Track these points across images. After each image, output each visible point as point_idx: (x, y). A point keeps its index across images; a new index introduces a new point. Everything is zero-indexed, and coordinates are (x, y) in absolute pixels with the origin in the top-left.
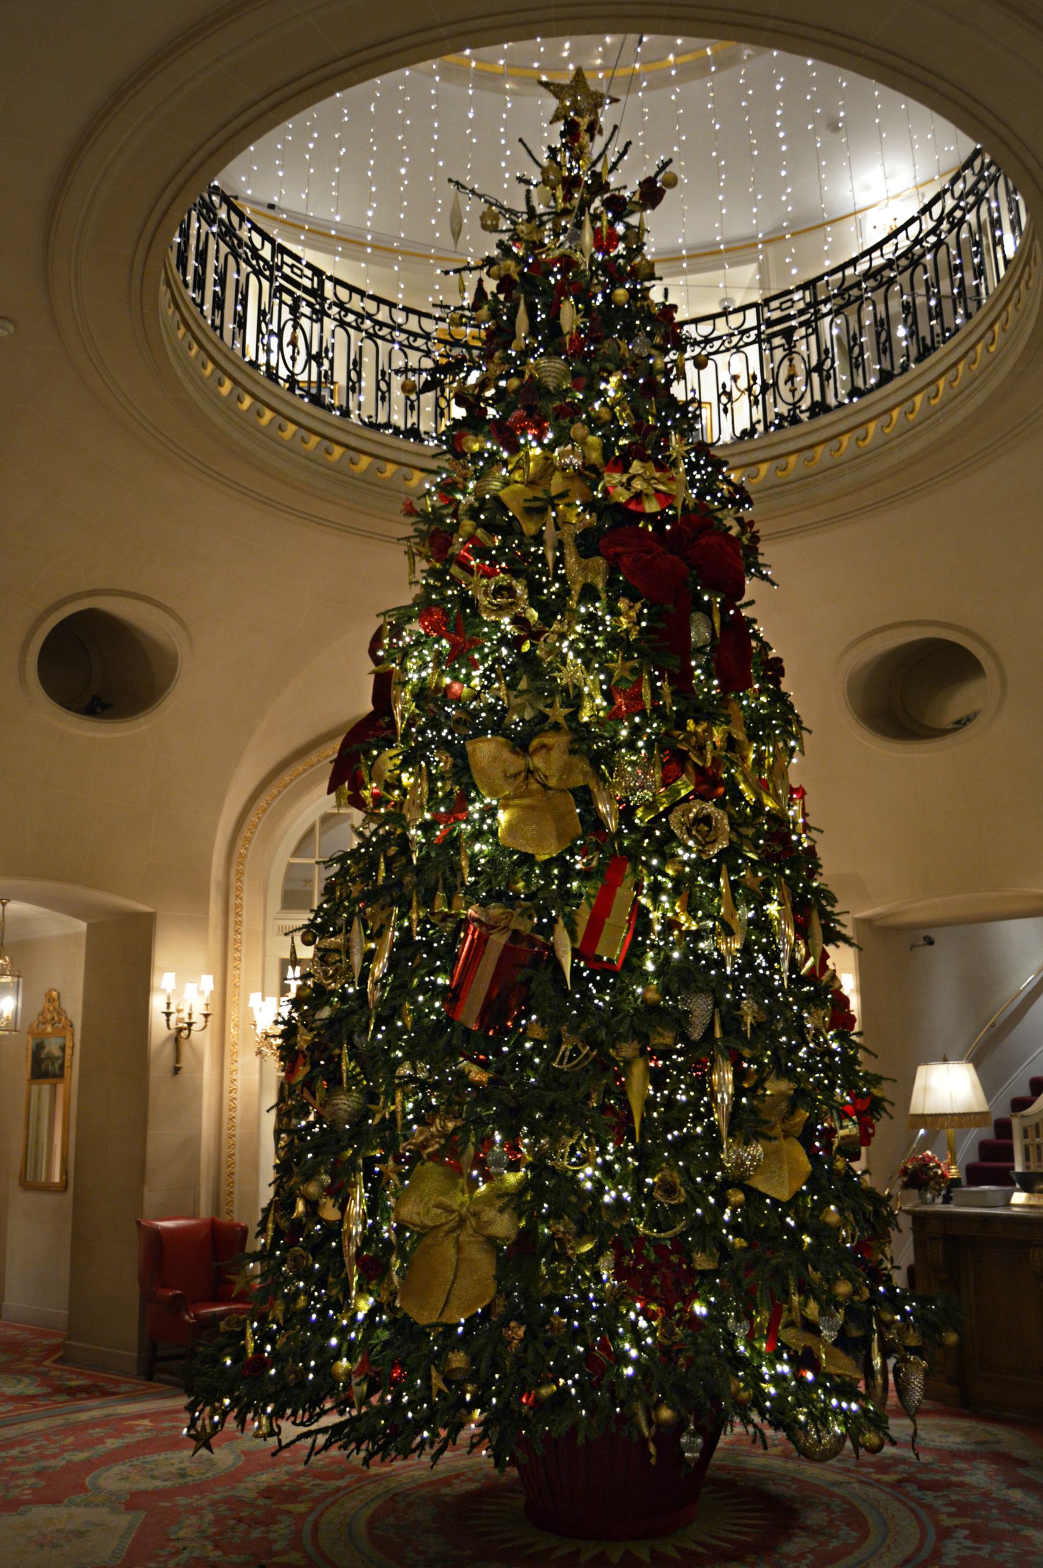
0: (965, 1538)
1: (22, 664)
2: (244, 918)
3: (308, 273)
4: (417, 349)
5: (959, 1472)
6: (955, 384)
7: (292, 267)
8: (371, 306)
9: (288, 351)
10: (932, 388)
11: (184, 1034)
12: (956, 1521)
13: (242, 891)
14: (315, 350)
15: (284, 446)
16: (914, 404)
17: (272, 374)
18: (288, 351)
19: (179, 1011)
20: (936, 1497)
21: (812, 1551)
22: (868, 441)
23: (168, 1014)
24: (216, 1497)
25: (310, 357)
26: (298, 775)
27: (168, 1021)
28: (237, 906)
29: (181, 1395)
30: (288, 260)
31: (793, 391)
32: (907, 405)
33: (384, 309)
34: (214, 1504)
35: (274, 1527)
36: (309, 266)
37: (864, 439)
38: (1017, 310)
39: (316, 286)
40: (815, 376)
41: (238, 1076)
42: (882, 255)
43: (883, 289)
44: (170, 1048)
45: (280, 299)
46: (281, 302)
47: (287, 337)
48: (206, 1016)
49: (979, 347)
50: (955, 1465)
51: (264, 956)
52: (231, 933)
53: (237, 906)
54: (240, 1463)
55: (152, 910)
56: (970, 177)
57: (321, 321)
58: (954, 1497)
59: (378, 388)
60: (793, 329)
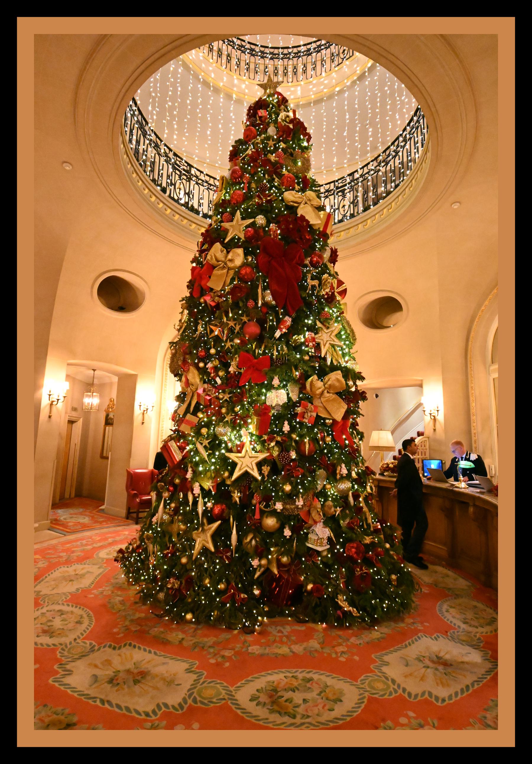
1: (92, 292)
3: (186, 165)
7: (180, 162)
8: (207, 178)
9: (178, 191)
10: (390, 206)
11: (145, 412)
14: (187, 191)
15: (174, 221)
25: (185, 193)
29: (132, 524)
30: (179, 160)
32: (381, 213)
33: (212, 180)
36: (186, 162)
40: (352, 205)
45: (175, 172)
46: (176, 173)
48: (65, 397)
57: (189, 181)
59: (209, 206)
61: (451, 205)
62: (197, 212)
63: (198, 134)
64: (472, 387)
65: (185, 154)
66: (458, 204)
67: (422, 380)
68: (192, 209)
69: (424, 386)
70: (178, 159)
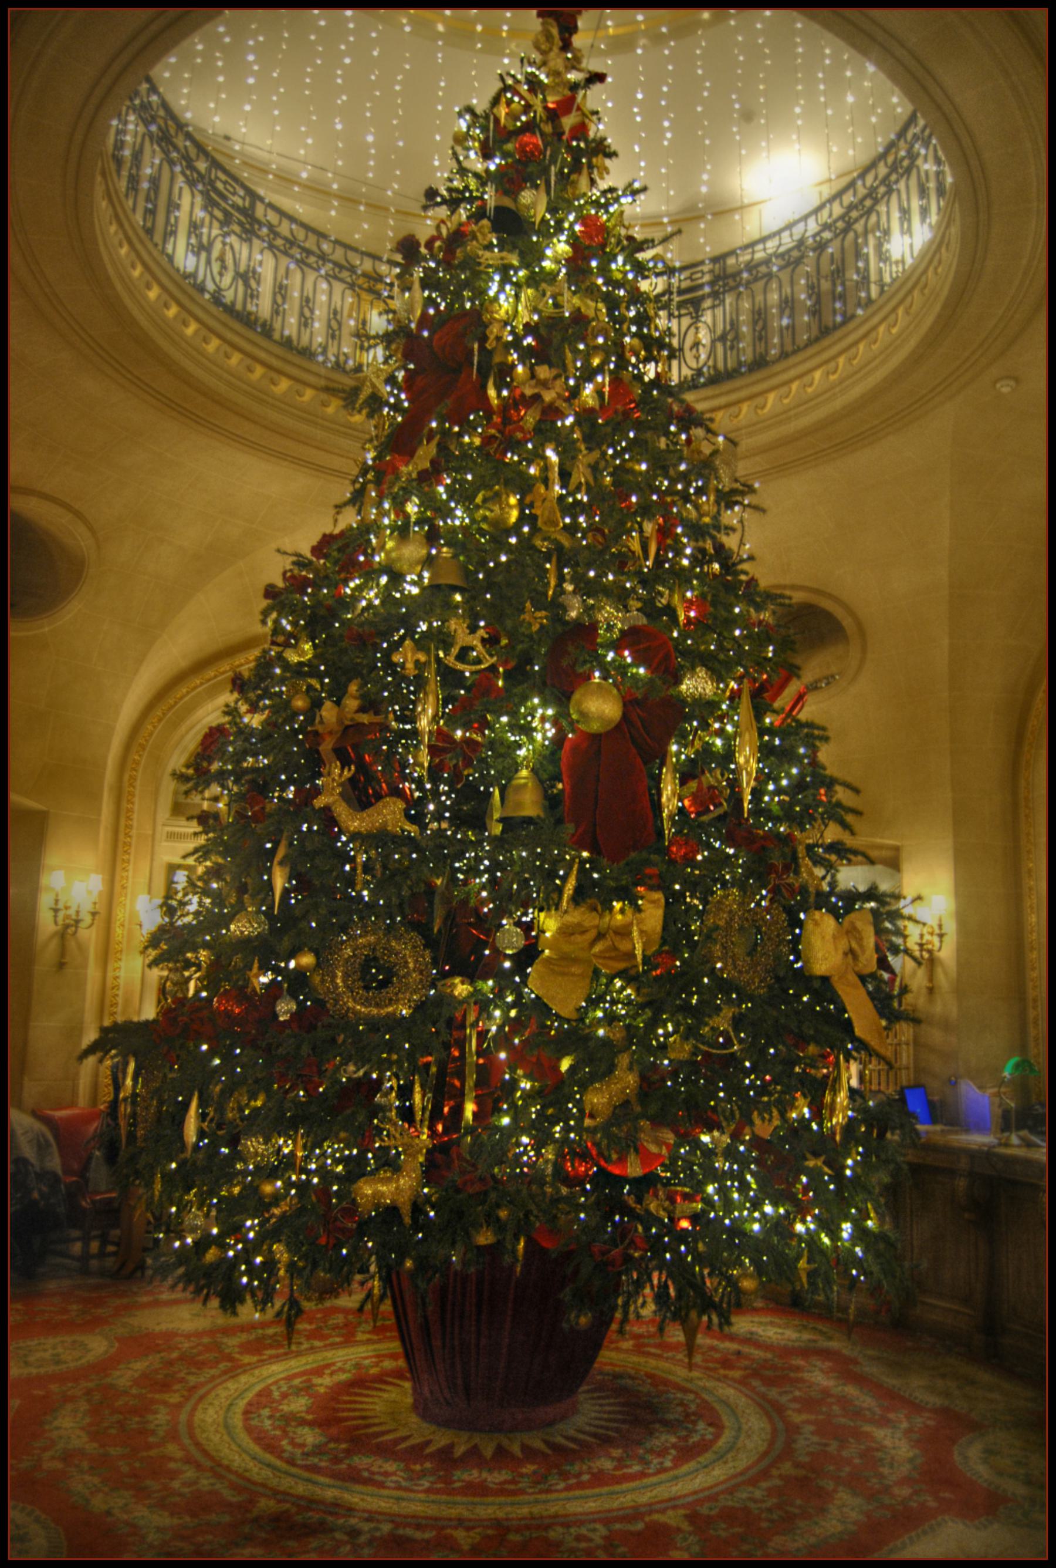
0: (813, 1433)
2: (135, 823)
4: (342, 280)
5: (798, 1369)
6: (855, 362)
7: (225, 183)
8: (301, 234)
11: (71, 930)
12: (804, 1417)
13: (133, 796)
14: (204, 255)
16: (813, 379)
17: (202, 289)
18: (216, 267)
19: (67, 908)
20: (781, 1394)
21: (674, 1446)
22: (766, 411)
23: (56, 911)
24: (90, 1385)
25: (238, 275)
26: (195, 688)
27: (55, 917)
28: (128, 810)
31: (697, 358)
34: (88, 1392)
35: (150, 1417)
37: (763, 407)
38: (923, 294)
39: (247, 204)
41: (122, 973)
42: (765, 249)
43: (789, 269)
44: (54, 945)
47: (215, 254)
49: (881, 329)
50: (794, 1362)
51: (152, 860)
52: (121, 836)
53: (128, 810)
54: (113, 1350)
55: (44, 808)
56: (882, 170)
58: (797, 1393)
60: (703, 298)
61: (995, 382)
62: (267, 331)
63: (372, 163)
64: (1030, 871)
65: (271, 177)
66: (1012, 383)
67: (897, 849)
68: (247, 320)
69: (905, 866)
70: (221, 175)
